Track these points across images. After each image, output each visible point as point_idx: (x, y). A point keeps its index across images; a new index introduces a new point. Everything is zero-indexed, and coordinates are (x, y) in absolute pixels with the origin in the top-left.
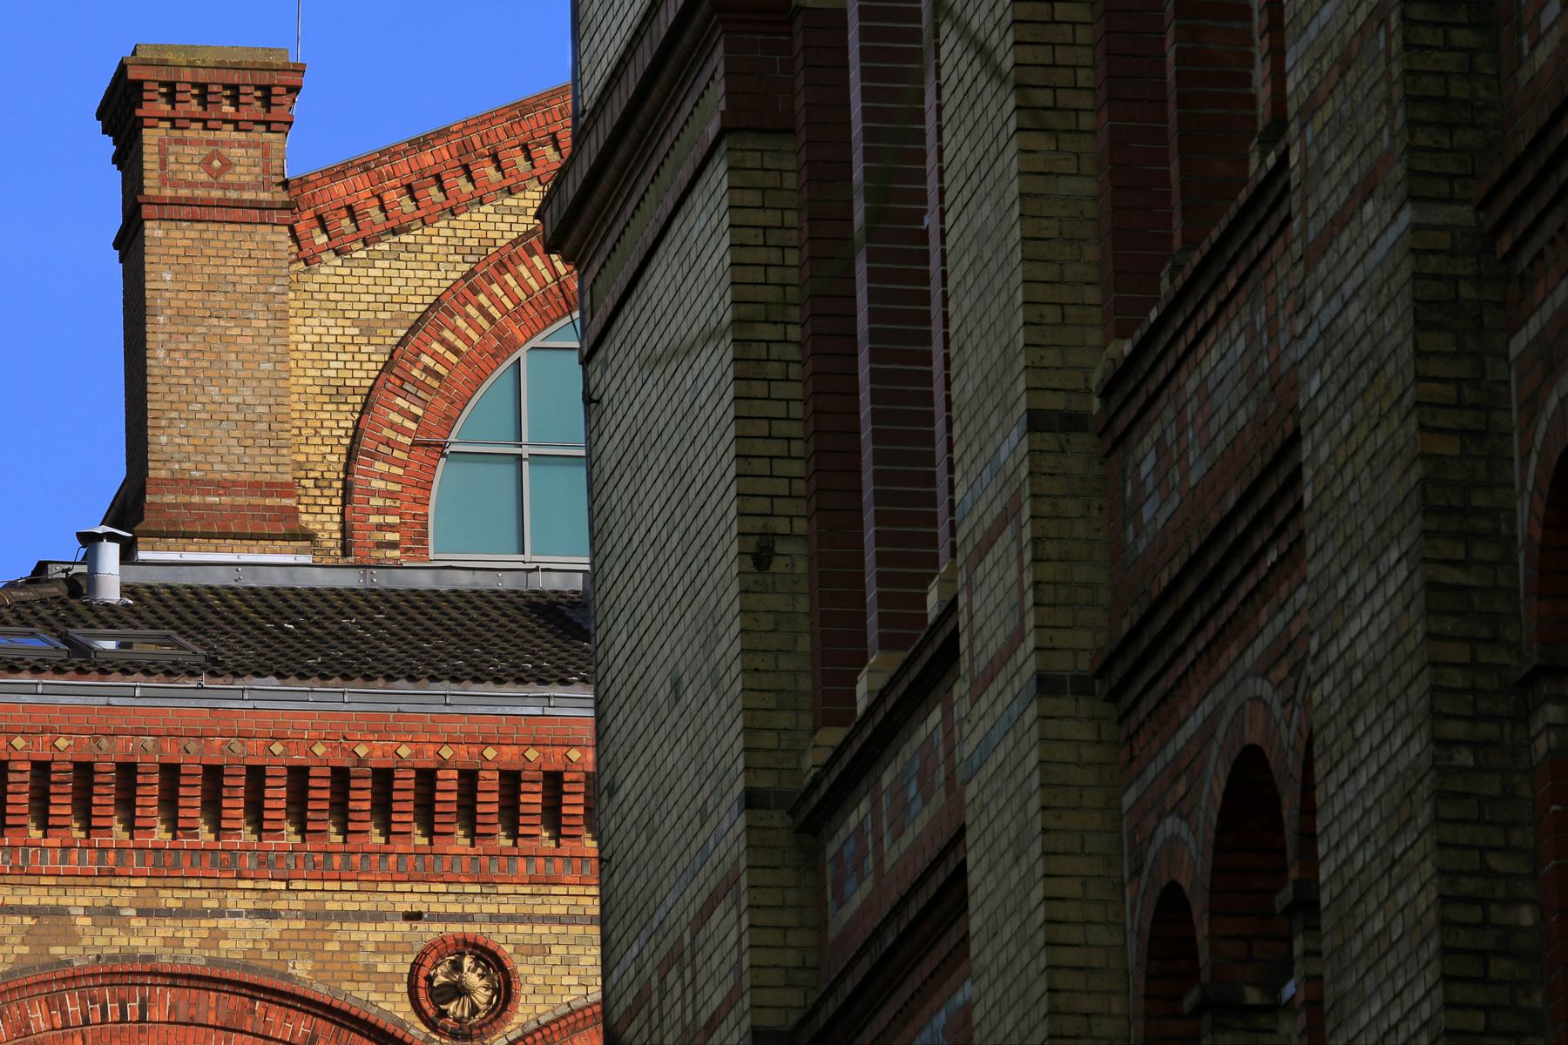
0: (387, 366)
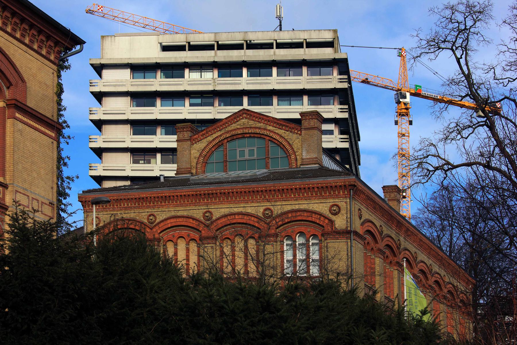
0: (200, 155)
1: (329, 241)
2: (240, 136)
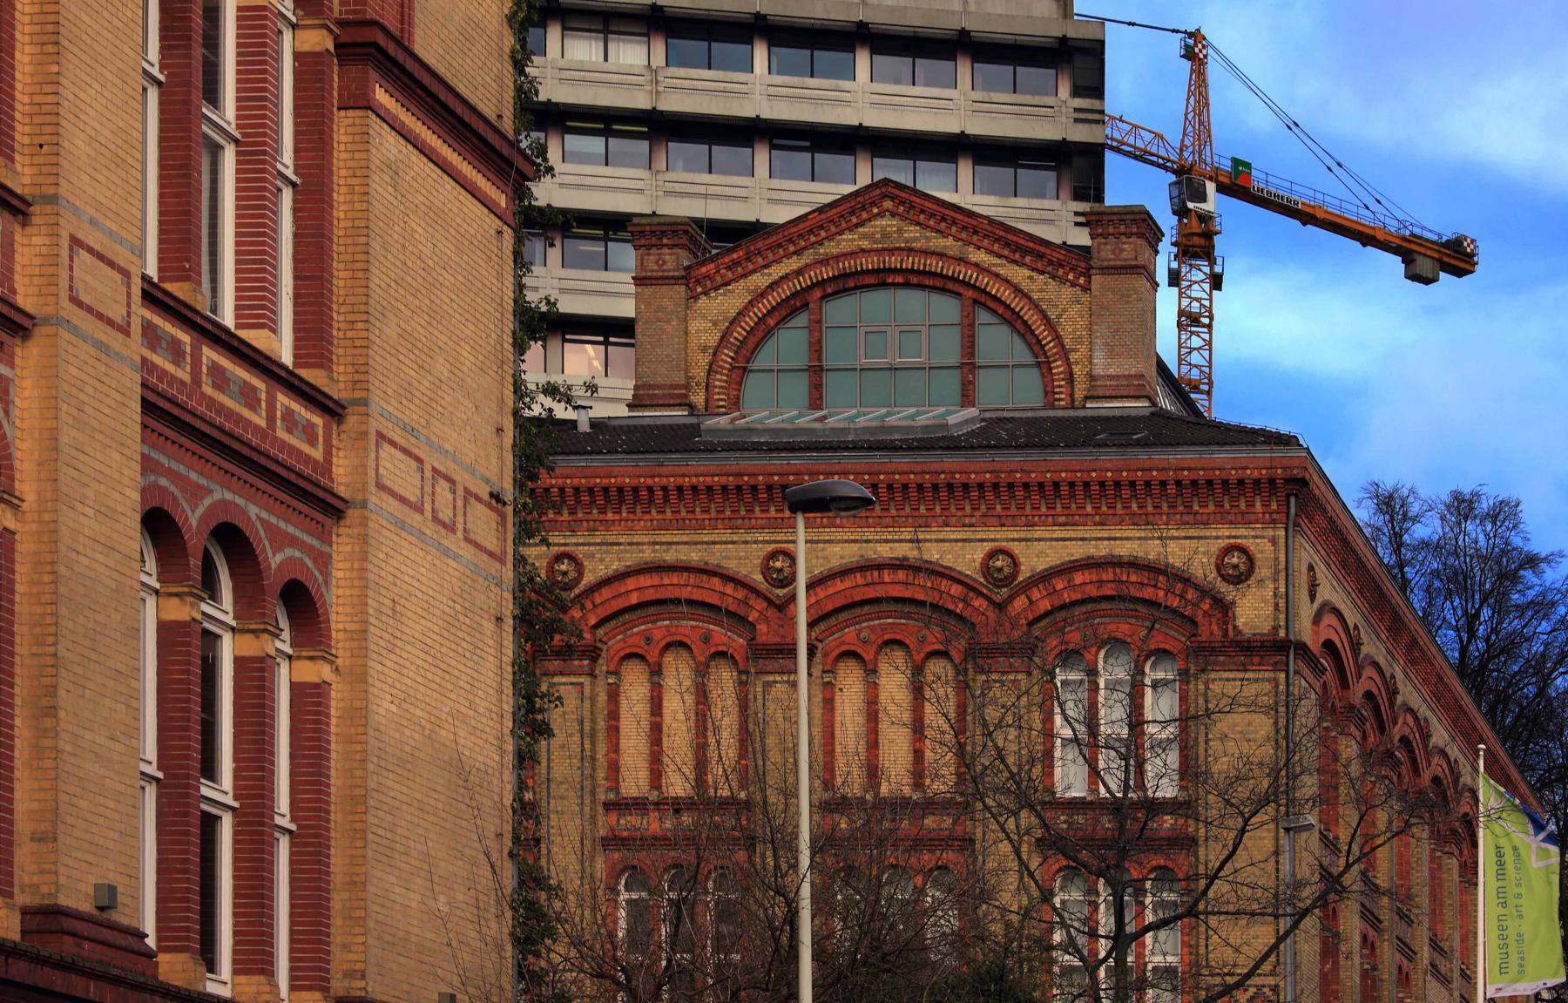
0: (722, 338)
1: (1212, 675)
2: (871, 280)
